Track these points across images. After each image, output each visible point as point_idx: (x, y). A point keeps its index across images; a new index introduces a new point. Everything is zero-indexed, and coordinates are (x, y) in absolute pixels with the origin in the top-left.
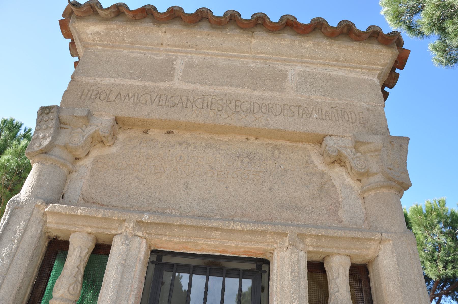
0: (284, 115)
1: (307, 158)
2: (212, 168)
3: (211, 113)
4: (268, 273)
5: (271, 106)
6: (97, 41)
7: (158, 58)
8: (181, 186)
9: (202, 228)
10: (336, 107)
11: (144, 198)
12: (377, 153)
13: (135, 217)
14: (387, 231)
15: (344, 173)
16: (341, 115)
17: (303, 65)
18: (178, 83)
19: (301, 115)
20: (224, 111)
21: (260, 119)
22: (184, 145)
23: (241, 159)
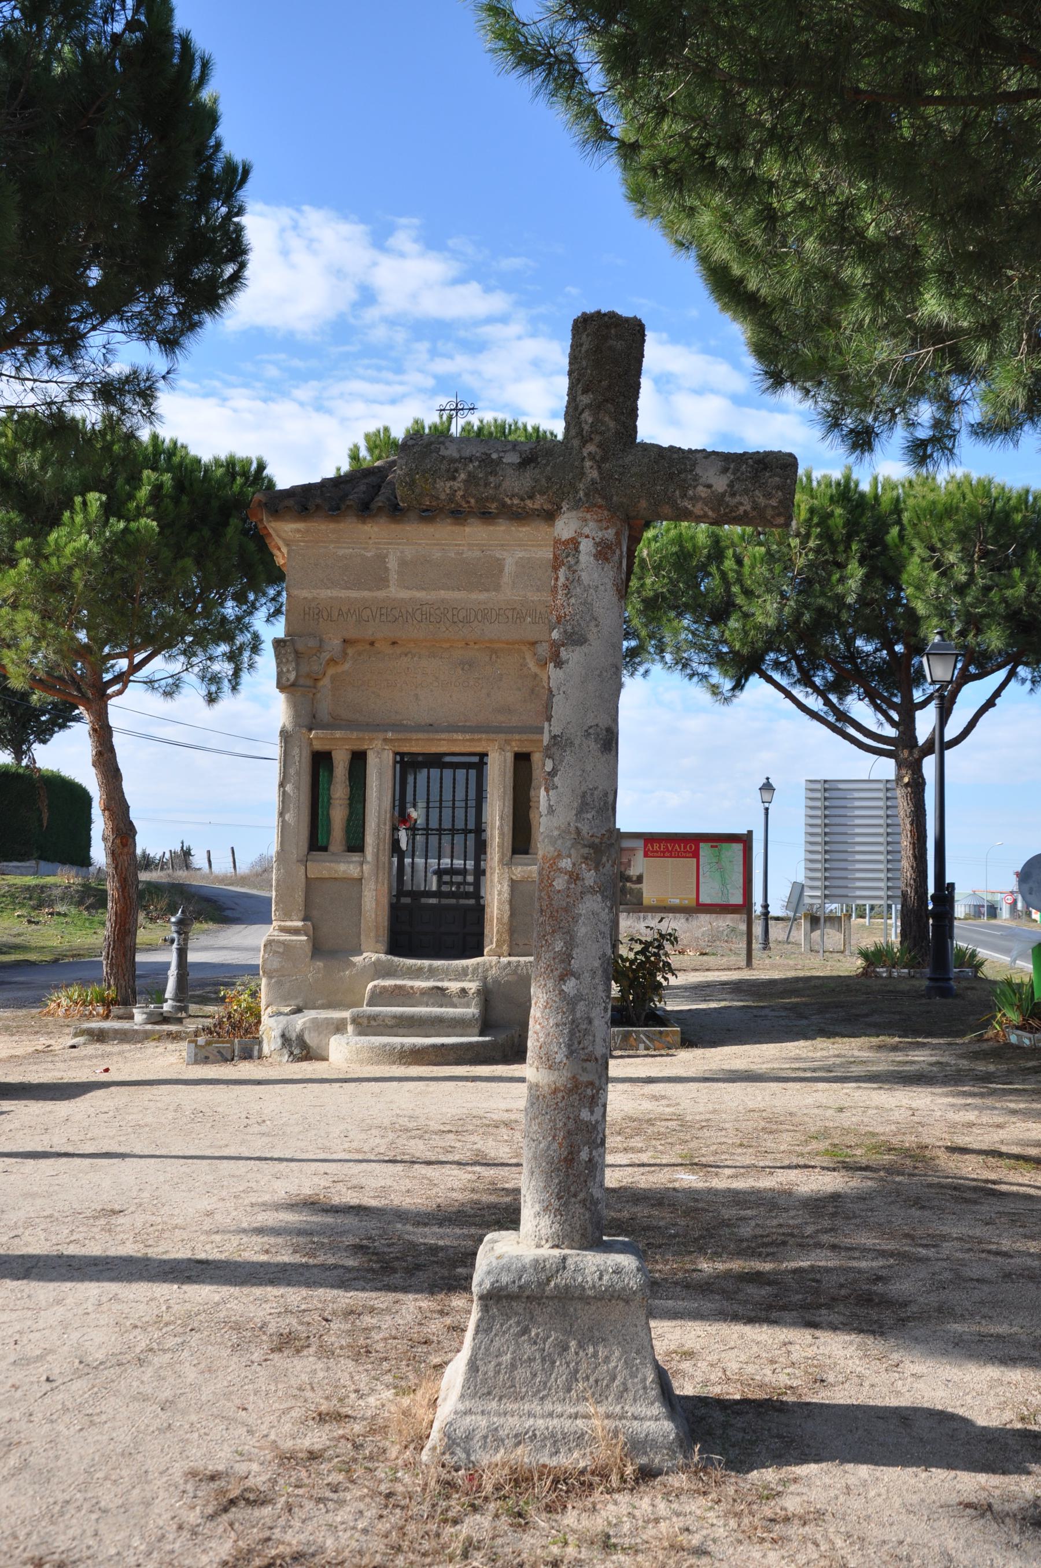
7: (369, 554)
13: (381, 736)
18: (395, 592)
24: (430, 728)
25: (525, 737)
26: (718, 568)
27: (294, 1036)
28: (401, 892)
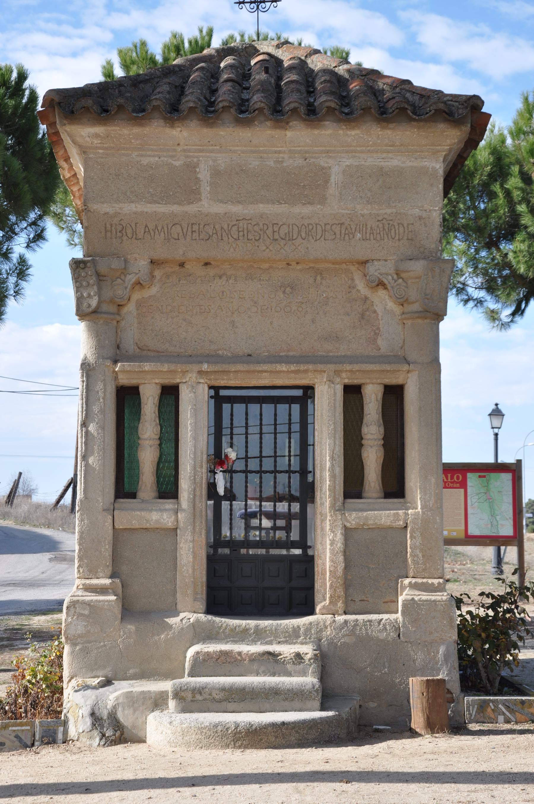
0: (325, 240)
1: (350, 282)
2: (256, 303)
3: (248, 244)
4: (312, 474)
5: (311, 227)
6: (96, 144)
7: (177, 163)
8: (228, 326)
9: (254, 372)
10: (382, 220)
11: (195, 341)
12: (417, 280)
13: (196, 368)
14: (415, 363)
15: (387, 297)
16: (387, 230)
17: (350, 155)
18: (207, 206)
19: (343, 236)
20: (261, 240)
21: (299, 248)
22: (224, 278)
23: (283, 289)
24: (249, 358)
25: (356, 367)
26: (502, 186)
27: (105, 714)
28: (217, 542)
